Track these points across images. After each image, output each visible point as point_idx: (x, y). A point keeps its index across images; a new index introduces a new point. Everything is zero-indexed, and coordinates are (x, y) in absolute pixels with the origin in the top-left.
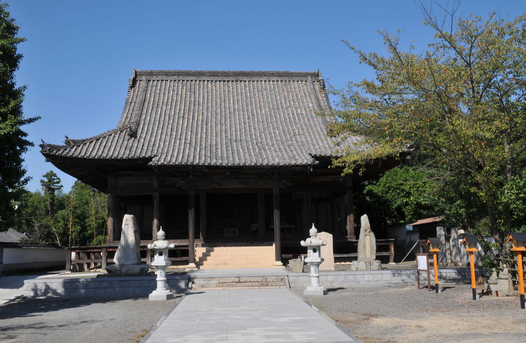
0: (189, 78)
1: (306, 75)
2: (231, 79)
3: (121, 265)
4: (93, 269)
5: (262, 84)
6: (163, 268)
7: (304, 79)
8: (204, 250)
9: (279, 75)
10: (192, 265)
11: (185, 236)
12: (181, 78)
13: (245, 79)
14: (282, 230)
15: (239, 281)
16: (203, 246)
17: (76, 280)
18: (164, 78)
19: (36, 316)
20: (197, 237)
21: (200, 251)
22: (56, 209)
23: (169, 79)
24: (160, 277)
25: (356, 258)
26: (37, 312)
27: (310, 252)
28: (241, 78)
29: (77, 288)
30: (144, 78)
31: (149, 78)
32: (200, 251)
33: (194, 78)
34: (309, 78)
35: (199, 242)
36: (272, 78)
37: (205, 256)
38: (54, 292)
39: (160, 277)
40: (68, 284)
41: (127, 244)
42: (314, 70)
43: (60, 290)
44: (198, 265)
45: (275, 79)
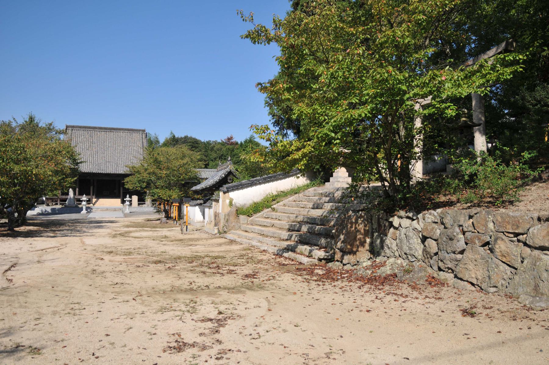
0: (90, 129)
1: (140, 130)
2: (108, 131)
3: (69, 204)
4: (170, 208)
5: (121, 134)
6: (85, 205)
7: (139, 132)
8: (96, 200)
9: (128, 130)
10: (91, 205)
11: (90, 195)
12: (86, 129)
13: (114, 131)
14: (123, 192)
15: (107, 210)
16: (95, 198)
17: (55, 208)
18: (79, 129)
19: (159, 231)
20: (93, 195)
21: (94, 200)
22: (412, 160)
23: (81, 129)
24: (84, 208)
25: (145, 204)
26: (54, 220)
27: (127, 202)
28: (112, 131)
29: (55, 211)
30: (70, 129)
31: (72, 129)
32: (94, 200)
33: (92, 130)
34: (141, 132)
35: (94, 197)
36: (125, 131)
37: (96, 202)
38: (48, 212)
39: (84, 208)
40: (53, 210)
41: (70, 198)
42: (143, 129)
43: (50, 211)
44: (94, 205)
45: (126, 131)
